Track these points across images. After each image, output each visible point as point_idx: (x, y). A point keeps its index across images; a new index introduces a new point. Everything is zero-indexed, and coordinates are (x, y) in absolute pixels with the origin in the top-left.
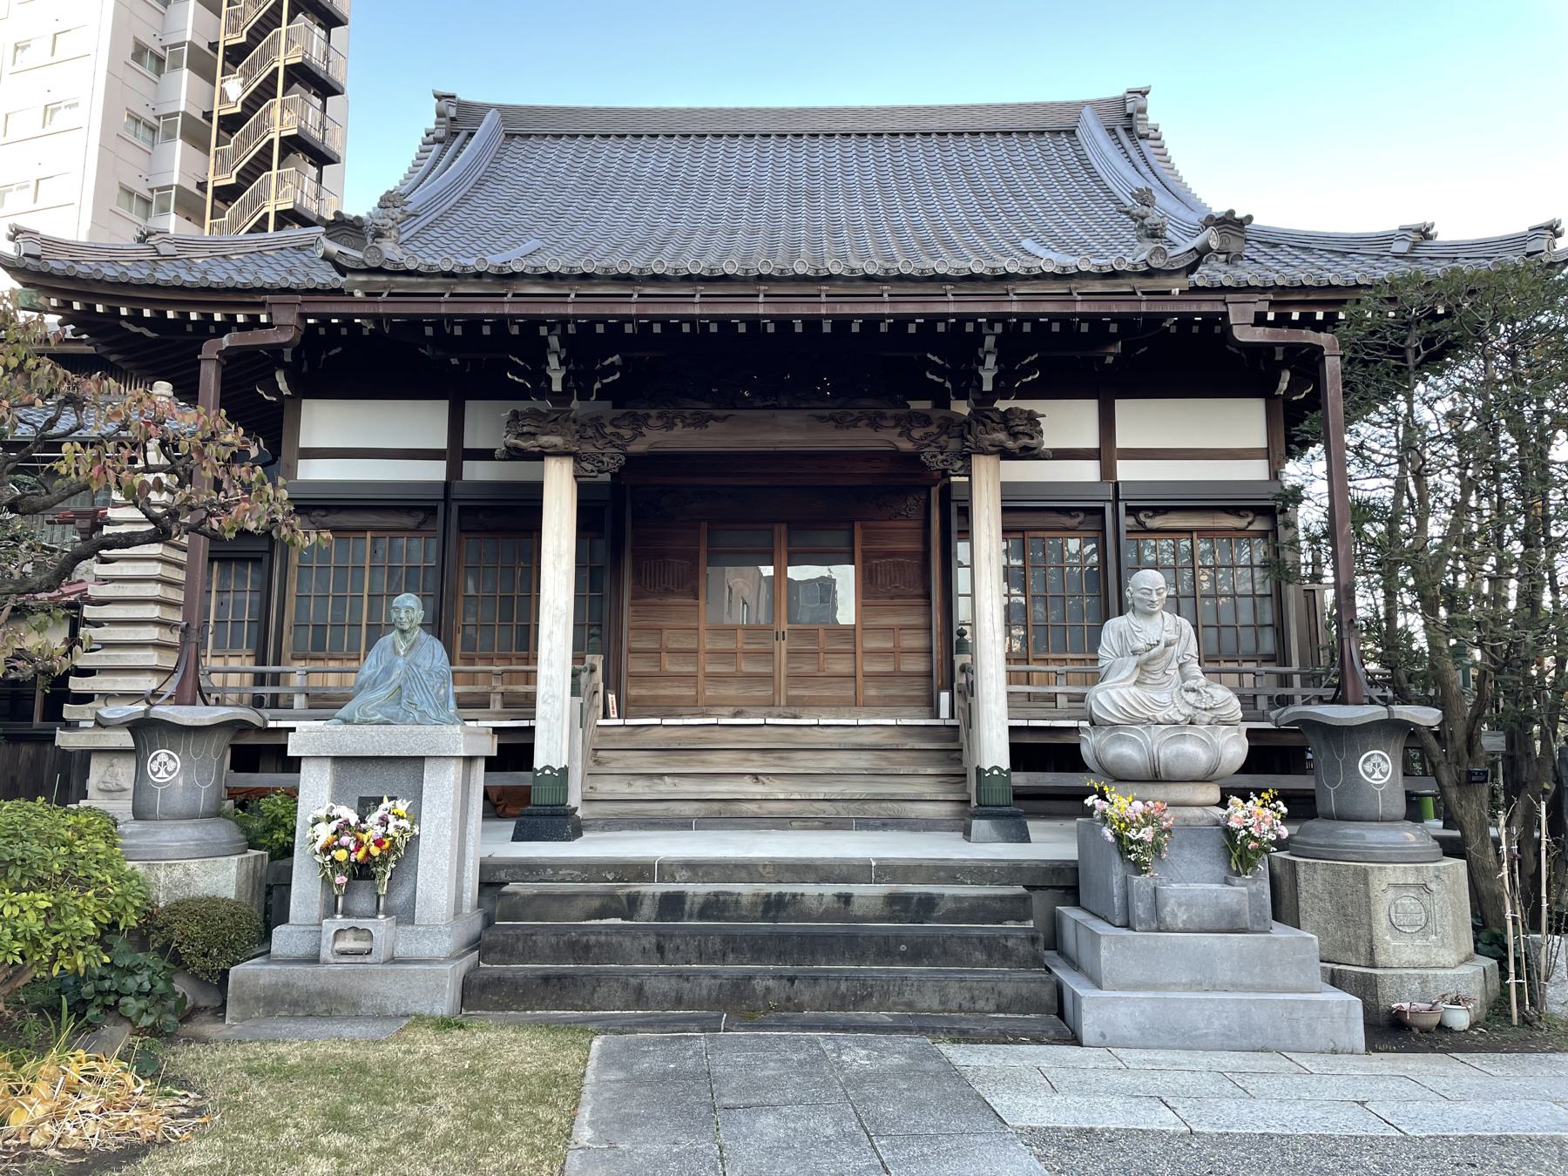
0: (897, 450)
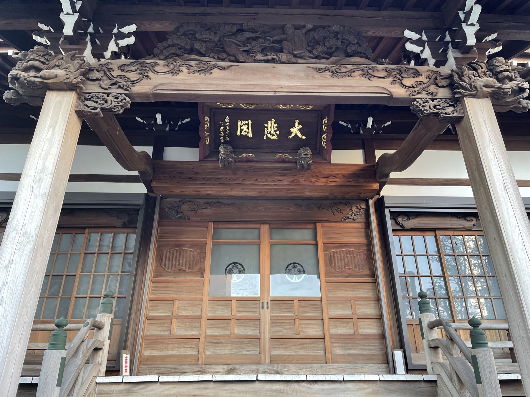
0: (391, 97)
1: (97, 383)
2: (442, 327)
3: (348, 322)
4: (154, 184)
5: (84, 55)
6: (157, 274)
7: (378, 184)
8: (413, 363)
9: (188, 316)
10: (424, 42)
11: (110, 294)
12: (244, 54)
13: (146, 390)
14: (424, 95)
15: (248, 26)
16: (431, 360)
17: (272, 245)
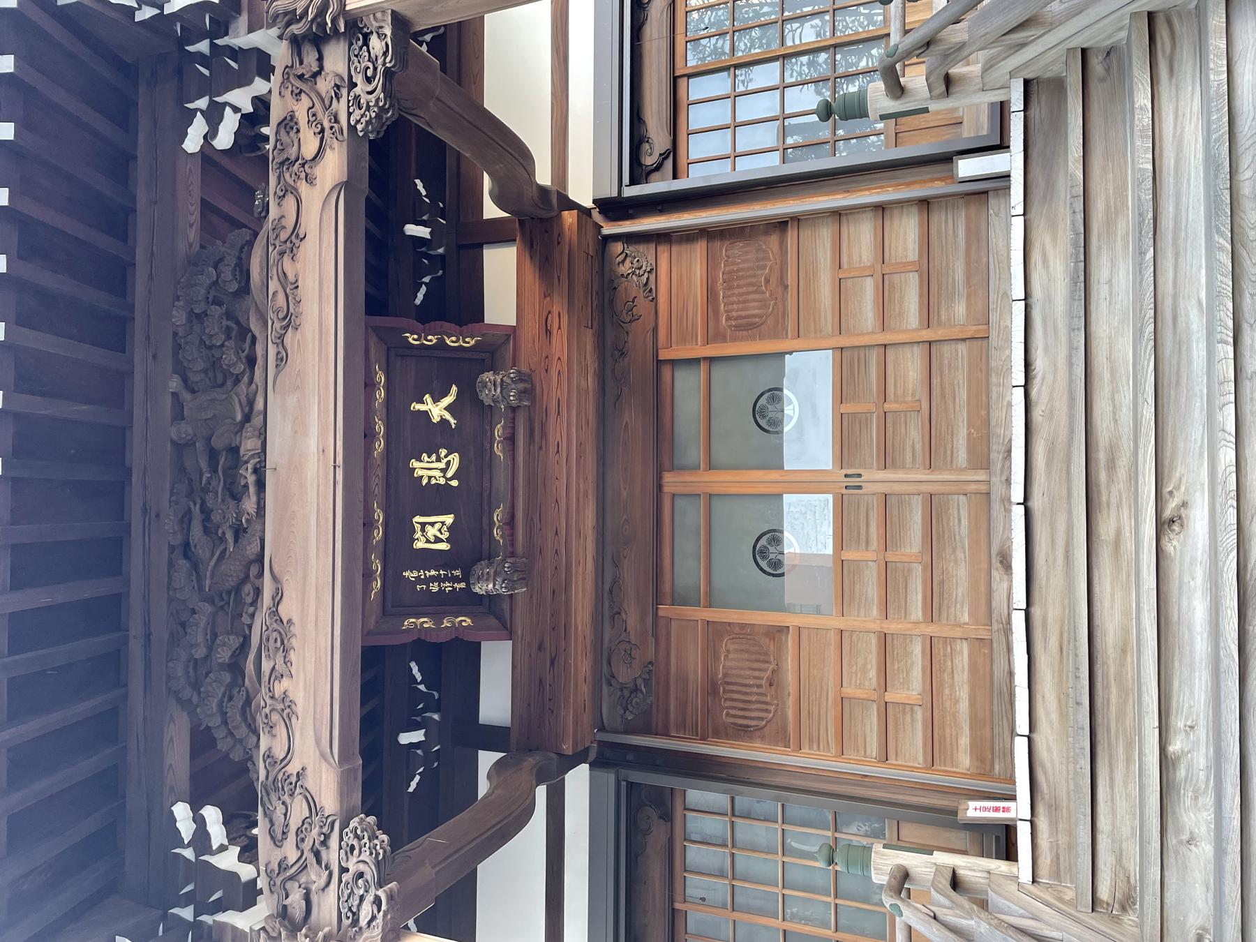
0: (347, 186)
1: (1034, 881)
2: (898, 66)
3: (892, 285)
4: (567, 748)
5: (247, 930)
6: (781, 738)
7: (565, 213)
8: (985, 133)
9: (879, 664)
10: (212, 104)
11: (825, 851)
12: (243, 541)
13: (1048, 765)
14: (341, 107)
15: (174, 533)
16: (976, 91)
17: (710, 467)
